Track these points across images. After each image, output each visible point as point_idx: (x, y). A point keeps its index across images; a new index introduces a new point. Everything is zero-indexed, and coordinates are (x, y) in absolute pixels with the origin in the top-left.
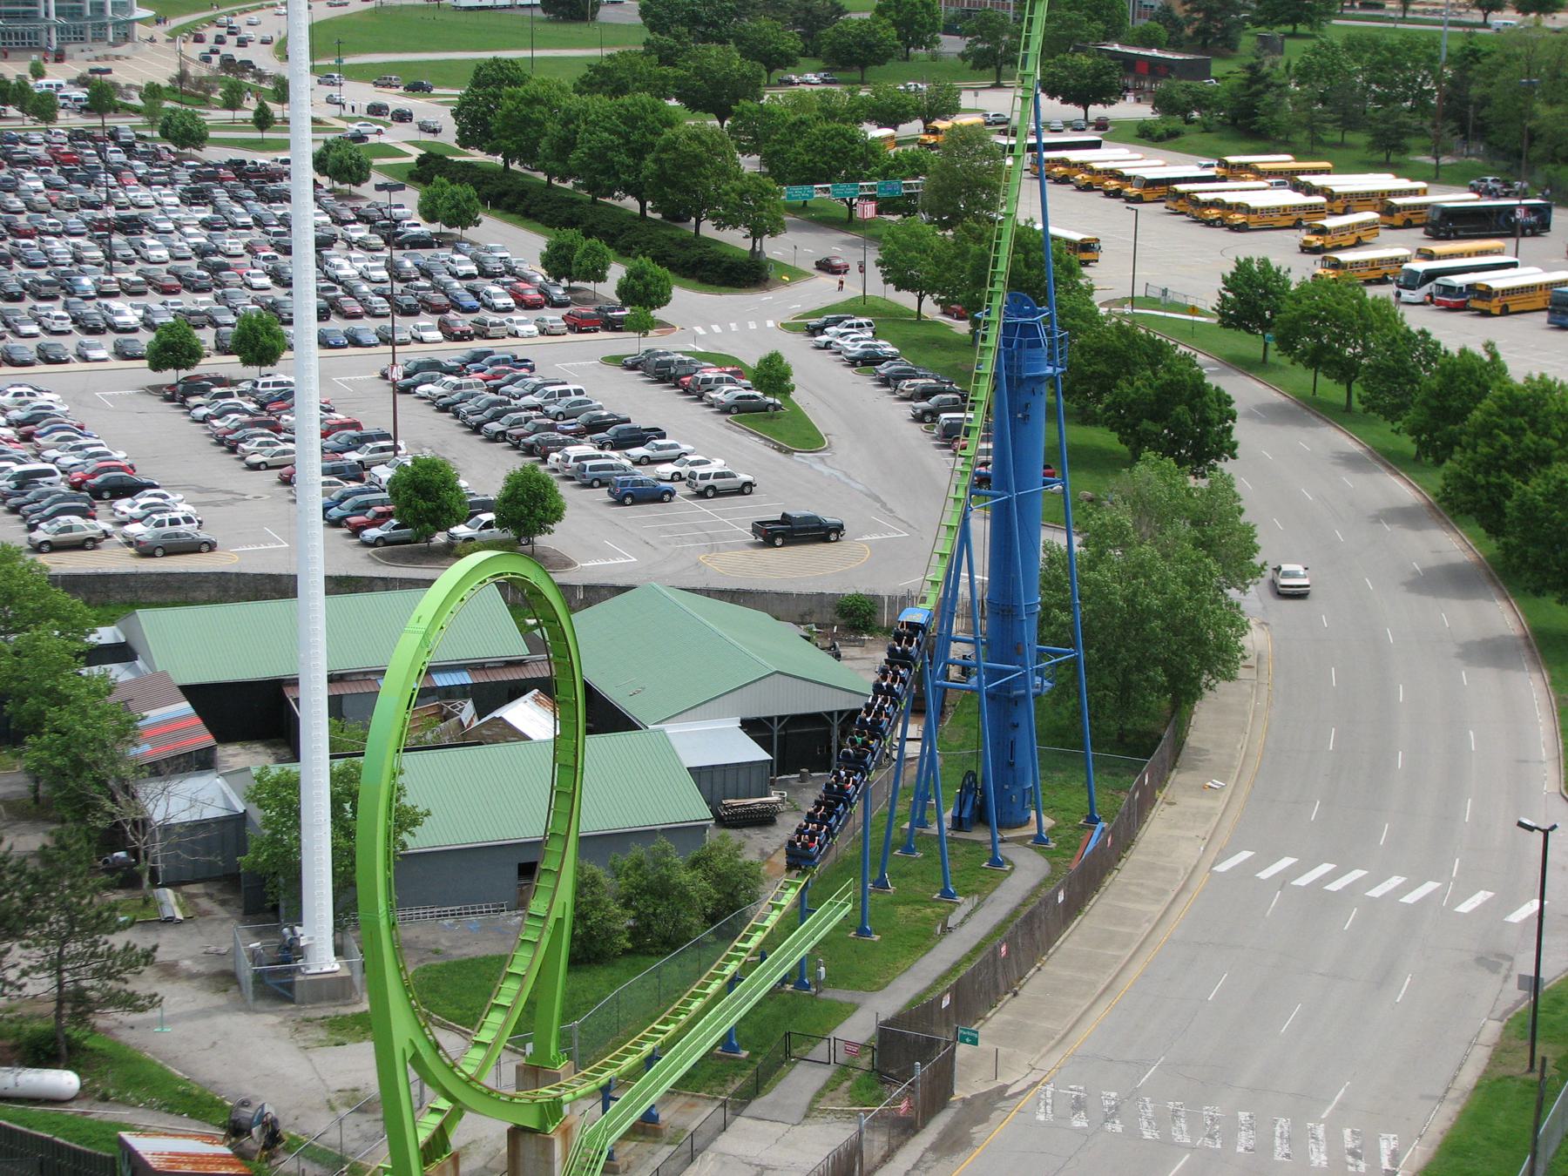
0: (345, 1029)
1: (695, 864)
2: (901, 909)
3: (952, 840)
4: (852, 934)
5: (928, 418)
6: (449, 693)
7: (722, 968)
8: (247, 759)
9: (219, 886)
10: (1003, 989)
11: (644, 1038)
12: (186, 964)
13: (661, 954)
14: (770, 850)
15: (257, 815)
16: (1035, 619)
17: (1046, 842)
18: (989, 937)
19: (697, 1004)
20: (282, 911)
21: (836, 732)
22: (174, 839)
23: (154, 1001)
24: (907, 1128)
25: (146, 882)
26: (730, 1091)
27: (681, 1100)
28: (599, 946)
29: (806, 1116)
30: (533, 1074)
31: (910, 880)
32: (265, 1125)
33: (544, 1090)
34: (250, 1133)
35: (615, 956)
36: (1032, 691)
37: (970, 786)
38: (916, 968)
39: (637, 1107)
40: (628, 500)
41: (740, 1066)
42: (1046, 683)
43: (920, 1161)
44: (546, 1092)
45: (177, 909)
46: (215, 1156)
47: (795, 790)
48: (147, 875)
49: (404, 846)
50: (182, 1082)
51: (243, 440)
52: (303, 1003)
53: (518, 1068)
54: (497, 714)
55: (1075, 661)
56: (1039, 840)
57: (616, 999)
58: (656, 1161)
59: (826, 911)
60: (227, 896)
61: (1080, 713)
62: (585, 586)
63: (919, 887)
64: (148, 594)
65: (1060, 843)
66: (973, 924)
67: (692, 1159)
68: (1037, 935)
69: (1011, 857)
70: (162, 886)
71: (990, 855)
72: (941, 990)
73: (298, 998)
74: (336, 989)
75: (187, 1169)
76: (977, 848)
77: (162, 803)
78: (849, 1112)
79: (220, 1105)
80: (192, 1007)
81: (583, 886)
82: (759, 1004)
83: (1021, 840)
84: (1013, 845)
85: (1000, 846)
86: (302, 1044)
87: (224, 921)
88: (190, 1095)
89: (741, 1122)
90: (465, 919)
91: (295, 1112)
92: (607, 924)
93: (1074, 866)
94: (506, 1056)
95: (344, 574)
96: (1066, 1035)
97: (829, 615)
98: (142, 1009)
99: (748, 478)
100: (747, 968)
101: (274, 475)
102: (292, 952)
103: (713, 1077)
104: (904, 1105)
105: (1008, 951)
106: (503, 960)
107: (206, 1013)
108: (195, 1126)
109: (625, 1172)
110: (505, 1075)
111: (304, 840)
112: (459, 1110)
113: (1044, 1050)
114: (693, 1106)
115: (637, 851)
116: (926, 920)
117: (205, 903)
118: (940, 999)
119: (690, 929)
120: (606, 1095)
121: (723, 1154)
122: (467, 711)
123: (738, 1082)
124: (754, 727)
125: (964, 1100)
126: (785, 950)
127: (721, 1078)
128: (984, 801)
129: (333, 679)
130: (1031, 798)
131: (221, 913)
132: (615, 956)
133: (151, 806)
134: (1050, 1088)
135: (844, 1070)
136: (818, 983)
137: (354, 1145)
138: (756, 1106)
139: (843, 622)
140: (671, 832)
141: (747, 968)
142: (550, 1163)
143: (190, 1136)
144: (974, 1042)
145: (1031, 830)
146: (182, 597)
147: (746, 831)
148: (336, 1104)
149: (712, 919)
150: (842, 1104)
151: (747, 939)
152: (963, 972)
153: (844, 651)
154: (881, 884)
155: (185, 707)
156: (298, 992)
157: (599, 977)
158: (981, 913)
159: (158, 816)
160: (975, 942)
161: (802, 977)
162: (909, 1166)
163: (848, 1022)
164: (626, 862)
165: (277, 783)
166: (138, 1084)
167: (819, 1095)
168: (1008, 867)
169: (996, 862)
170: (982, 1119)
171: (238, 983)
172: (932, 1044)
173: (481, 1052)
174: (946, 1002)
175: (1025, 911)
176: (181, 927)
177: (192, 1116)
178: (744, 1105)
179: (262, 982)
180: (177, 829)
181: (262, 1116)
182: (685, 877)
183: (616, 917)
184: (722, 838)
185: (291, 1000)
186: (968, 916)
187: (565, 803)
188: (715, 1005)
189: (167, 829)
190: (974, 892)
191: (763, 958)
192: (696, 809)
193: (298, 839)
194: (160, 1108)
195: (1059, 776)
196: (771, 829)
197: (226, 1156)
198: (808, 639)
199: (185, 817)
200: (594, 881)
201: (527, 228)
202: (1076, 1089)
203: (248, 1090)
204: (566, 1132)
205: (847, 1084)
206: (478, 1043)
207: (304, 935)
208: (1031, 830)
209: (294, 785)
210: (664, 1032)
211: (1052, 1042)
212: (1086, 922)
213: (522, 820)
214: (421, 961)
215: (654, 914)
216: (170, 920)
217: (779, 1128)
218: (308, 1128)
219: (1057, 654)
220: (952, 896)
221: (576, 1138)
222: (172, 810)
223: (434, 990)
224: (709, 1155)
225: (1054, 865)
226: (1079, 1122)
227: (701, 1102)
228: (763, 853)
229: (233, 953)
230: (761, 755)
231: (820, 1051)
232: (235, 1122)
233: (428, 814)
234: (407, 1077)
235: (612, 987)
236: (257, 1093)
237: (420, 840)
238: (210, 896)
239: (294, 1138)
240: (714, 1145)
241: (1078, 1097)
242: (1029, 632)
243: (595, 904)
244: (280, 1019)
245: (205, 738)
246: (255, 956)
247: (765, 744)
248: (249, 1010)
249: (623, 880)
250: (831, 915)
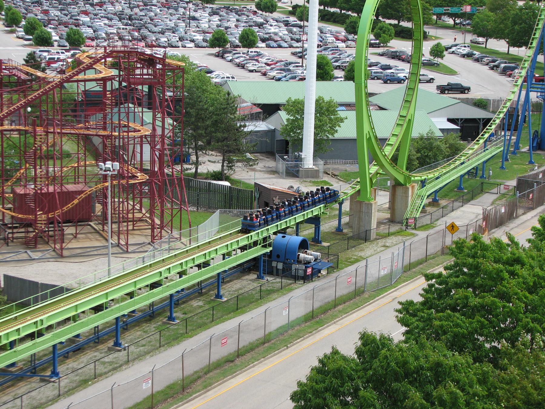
5: (495, 68)
40: (389, 82)
51: (247, 63)
67: (453, 211)
73: (300, 176)
99: (433, 77)
101: (259, 74)
102: (299, 159)
117: (261, 157)
120: (423, 183)
138: (472, 202)
142: (407, 197)
156: (300, 174)
185: (298, 177)
201: (335, 26)
207: (303, 155)
248: (283, 178)
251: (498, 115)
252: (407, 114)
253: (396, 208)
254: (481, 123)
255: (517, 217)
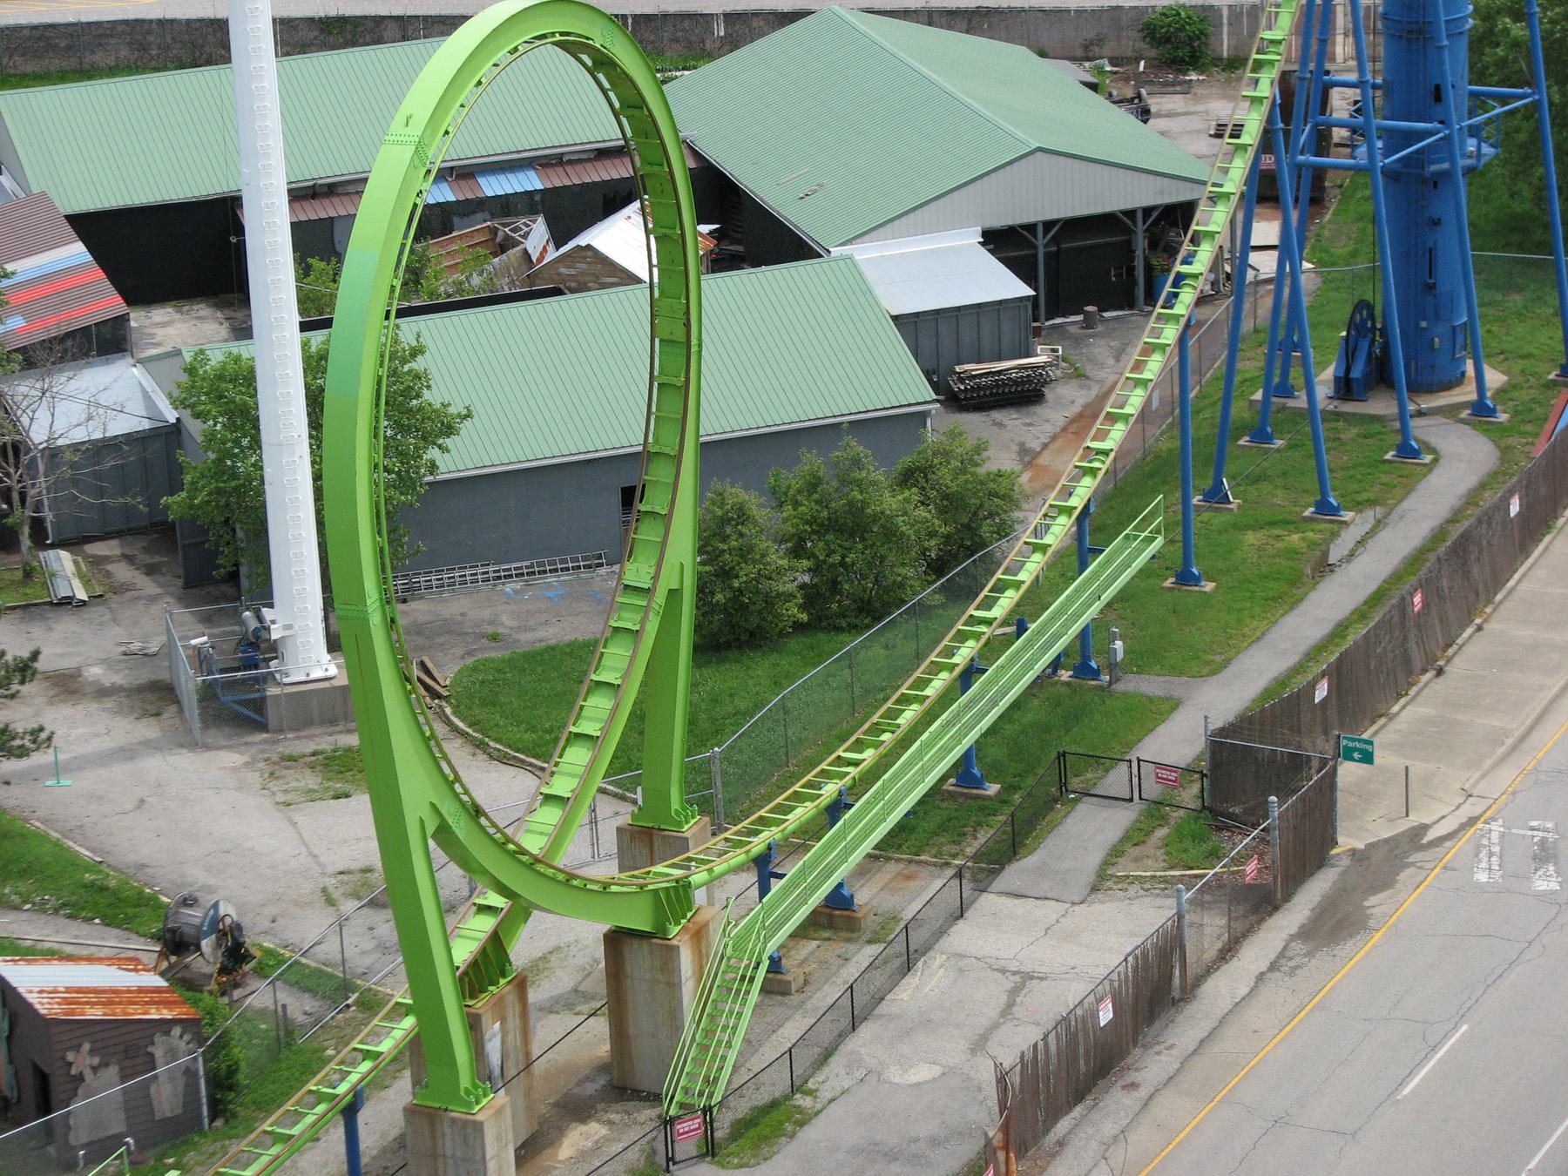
0: (341, 770)
1: (907, 478)
2: (1251, 538)
3: (1338, 415)
4: (1168, 583)
6: (506, 206)
7: (922, 683)
8: (181, 330)
9: (142, 542)
10: (1417, 664)
11: (824, 773)
12: (94, 672)
13: (856, 629)
14: (1035, 445)
15: (196, 429)
16: (1464, 43)
17: (1491, 412)
18: (1396, 578)
19: (909, 715)
20: (245, 583)
21: (1141, 244)
22: (66, 472)
23: (40, 738)
24: (1261, 903)
25: (26, 542)
26: (970, 851)
27: (892, 868)
28: (754, 621)
29: (1095, 889)
30: (644, 841)
31: (1266, 487)
32: (222, 934)
33: (659, 868)
34: (198, 948)
35: (781, 634)
36: (1463, 163)
37: (1362, 324)
38: (1274, 635)
39: (813, 889)
41: (987, 809)
42: (1487, 150)
43: (1281, 955)
44: (665, 872)
45: (76, 583)
46: (141, 990)
47: (1077, 341)
48: (26, 530)
49: (433, 467)
50: (88, 868)
52: (281, 731)
53: (618, 829)
54: (582, 240)
55: (1536, 105)
56: (1481, 409)
57: (783, 707)
58: (851, 972)
59: (1120, 550)
60: (157, 559)
61: (1547, 187)
62: (725, 15)
63: (1280, 497)
64: (18, 59)
65: (1516, 413)
66: (1372, 556)
67: (908, 967)
68: (1475, 570)
69: (1434, 441)
70: (53, 546)
71: (1398, 439)
72: (1317, 669)
74: (325, 707)
75: (95, 1013)
76: (1376, 427)
77: (43, 416)
78: (1165, 880)
79: (151, 902)
80: (106, 744)
81: (709, 540)
82: (1016, 705)
83: (1451, 411)
84: (1440, 420)
85: (1415, 424)
86: (281, 798)
87: (152, 599)
88: (103, 889)
89: (989, 902)
90: (540, 581)
91: (273, 910)
92: (764, 585)
93: (1539, 450)
94: (606, 807)
95: (333, 13)
96: (1524, 738)
97: (1131, 43)
98: (22, 753)
100: (993, 649)
102: (258, 649)
103: (942, 829)
104: (1251, 867)
105: (1426, 604)
106: (584, 653)
107: (127, 753)
108: (111, 940)
109: (801, 991)
110: (592, 852)
111: (268, 472)
112: (520, 910)
113: (1488, 763)
114: (909, 878)
115: (811, 461)
116: (1293, 554)
117: (122, 572)
118: (1312, 686)
119: (902, 586)
120: (765, 868)
121: (961, 956)
122: (536, 236)
123: (984, 836)
124: (1004, 242)
125: (1353, 852)
126: (1053, 618)
127: (955, 830)
128: (1386, 347)
129: (298, 195)
130: (1466, 340)
131: (148, 586)
132: (781, 634)
133: (25, 420)
134: (1497, 827)
135: (1156, 810)
136: (1112, 667)
137: (367, 961)
138: (1013, 875)
139: (1154, 53)
140: (865, 427)
141: (993, 649)
142: (674, 985)
143: (100, 960)
144: (1367, 758)
145: (1468, 393)
146: (70, 63)
147: (997, 415)
148: (336, 894)
149: (938, 567)
150: (1152, 867)
151: (988, 604)
152: (1350, 639)
153: (1154, 103)
154: (1216, 496)
155: (76, 252)
157: (747, 677)
158: (1384, 535)
159: (38, 434)
160: (1372, 587)
161: (1085, 657)
162: (1263, 966)
163: (1163, 730)
164: (793, 480)
165: (220, 377)
166: (23, 873)
167: (1116, 852)
168: (1428, 458)
169: (1407, 451)
170: (1384, 882)
171: (178, 702)
172: (1298, 764)
173: (552, 807)
174: (1321, 692)
175: (1456, 532)
176: (86, 613)
177: (108, 922)
178: (994, 873)
179: (214, 697)
180: (68, 456)
181: (216, 920)
182: (890, 502)
183: (779, 571)
184: (953, 435)
185: (262, 727)
186: (1361, 542)
187: (674, 401)
188: (937, 717)
189: (53, 454)
190: (1372, 503)
191: (1021, 629)
192: (903, 383)
193: (258, 467)
194: (56, 911)
195: (1516, 299)
196: (1037, 409)
197: (158, 990)
198: (1094, 87)
199: (79, 435)
200: (742, 515)
202: (1543, 827)
203: (197, 877)
204: (699, 936)
205: (1162, 832)
206: (549, 798)
207: (277, 622)
208: (1468, 393)
209: (247, 378)
210: (856, 763)
211: (1501, 751)
212: (1559, 546)
213: (613, 423)
214: (470, 653)
215: (842, 564)
216: (67, 602)
217: (1050, 910)
218: (291, 936)
219: (1504, 100)
220: (1334, 511)
221: (716, 941)
222: (60, 427)
223: (490, 702)
224: (936, 959)
225: (1505, 451)
226: (1547, 882)
227: (924, 872)
228: (1024, 451)
229: (168, 650)
230: (1023, 290)
231: (1116, 780)
232: (173, 931)
233: (468, 416)
234: (425, 859)
235: (777, 685)
236: (212, 881)
237: (455, 459)
238: (130, 559)
239: (270, 953)
240: (945, 942)
241: (1543, 842)
242: (1455, 67)
243: (745, 553)
244: (246, 758)
245: (109, 302)
246: (201, 659)
247: (1023, 269)
248: (194, 746)
249: (788, 510)
250: (1131, 555)
251: (1139, 366)
252: (656, 578)
253: (631, 1031)
254: (1141, 228)
255: (1190, 990)
